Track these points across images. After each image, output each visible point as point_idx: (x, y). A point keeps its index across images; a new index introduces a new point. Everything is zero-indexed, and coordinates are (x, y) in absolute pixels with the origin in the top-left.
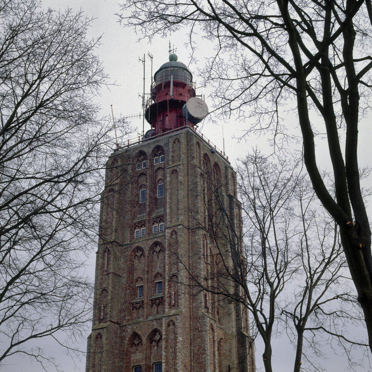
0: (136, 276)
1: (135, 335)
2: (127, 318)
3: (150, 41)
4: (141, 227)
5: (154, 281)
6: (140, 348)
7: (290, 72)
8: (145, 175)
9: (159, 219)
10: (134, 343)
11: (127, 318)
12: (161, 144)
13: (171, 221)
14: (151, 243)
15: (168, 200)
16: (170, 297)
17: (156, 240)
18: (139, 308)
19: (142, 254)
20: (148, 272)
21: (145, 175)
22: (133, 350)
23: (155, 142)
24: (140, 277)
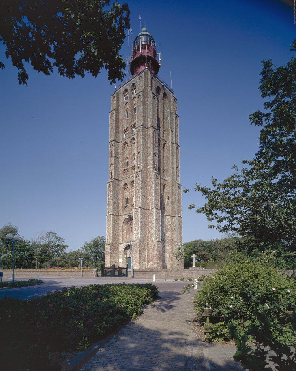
0: (125, 157)
1: (126, 184)
2: (122, 177)
3: (198, 186)
4: (127, 132)
5: (133, 158)
6: (128, 190)
7: (17, 32)
8: (128, 103)
9: (134, 126)
10: (125, 188)
11: (122, 177)
12: (134, 82)
13: (138, 125)
14: (131, 139)
15: (136, 116)
16: (144, 209)
17: (133, 137)
18: (127, 189)
19: (127, 146)
20: (130, 154)
21: (128, 103)
22: (125, 191)
23: (131, 82)
24: (127, 157)
